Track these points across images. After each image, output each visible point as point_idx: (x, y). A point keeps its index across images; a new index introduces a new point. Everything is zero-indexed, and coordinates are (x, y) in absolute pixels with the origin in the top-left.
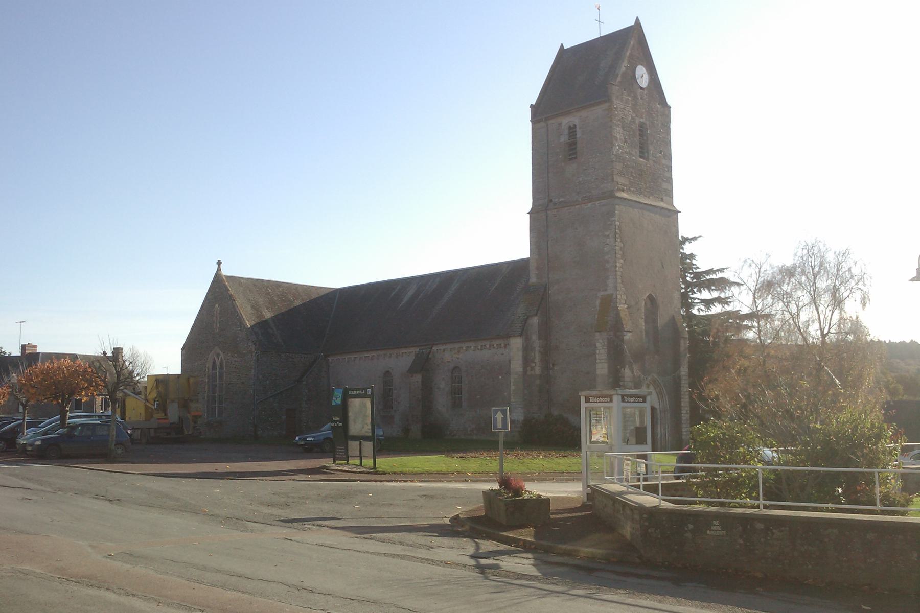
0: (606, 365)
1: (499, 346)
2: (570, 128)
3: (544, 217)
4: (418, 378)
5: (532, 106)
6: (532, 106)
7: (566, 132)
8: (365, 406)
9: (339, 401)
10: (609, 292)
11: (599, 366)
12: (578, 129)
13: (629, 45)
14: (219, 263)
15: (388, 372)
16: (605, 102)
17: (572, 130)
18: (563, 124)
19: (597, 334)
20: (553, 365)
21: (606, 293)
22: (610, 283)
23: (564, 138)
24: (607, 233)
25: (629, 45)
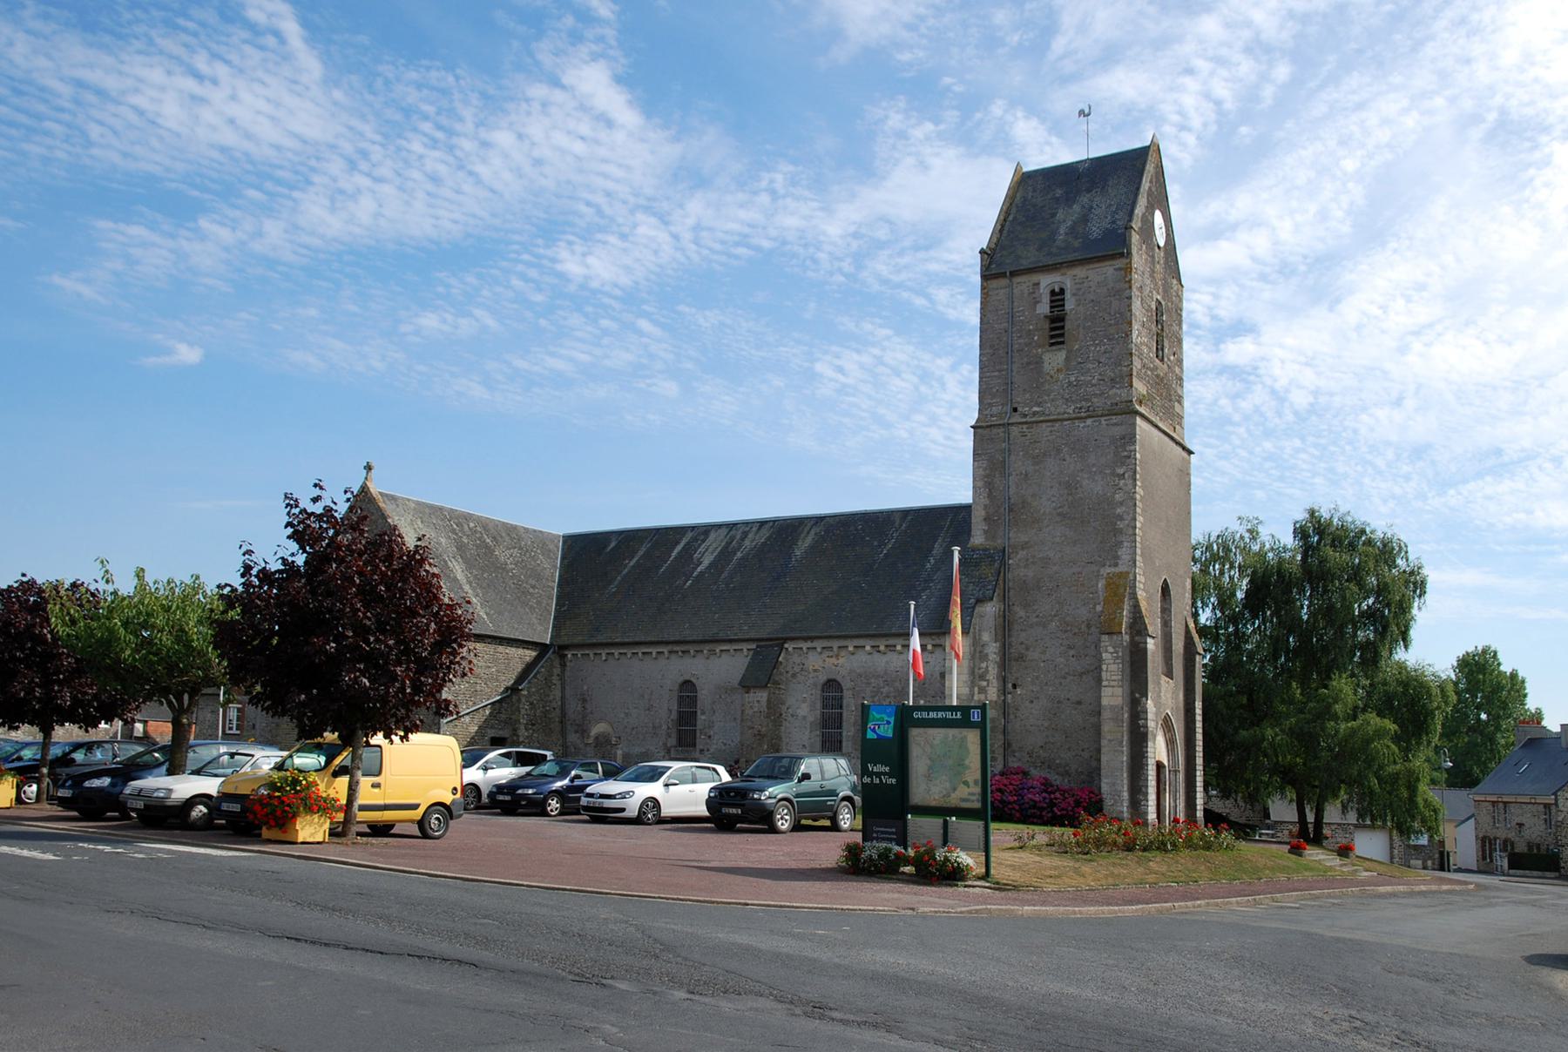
0: (1119, 691)
1: (891, 648)
2: (1053, 293)
3: (990, 435)
4: (762, 696)
5: (982, 252)
6: (982, 252)
7: (1046, 299)
8: (962, 744)
9: (887, 731)
10: (1122, 568)
11: (1106, 692)
12: (1068, 295)
13: (1127, 176)
14: (369, 468)
15: (829, 681)
16: (1122, 255)
17: (1057, 297)
18: (1043, 285)
19: (1105, 638)
20: (1014, 686)
21: (1117, 570)
22: (1124, 553)
23: (1044, 308)
24: (1121, 471)
25: (1127, 176)
